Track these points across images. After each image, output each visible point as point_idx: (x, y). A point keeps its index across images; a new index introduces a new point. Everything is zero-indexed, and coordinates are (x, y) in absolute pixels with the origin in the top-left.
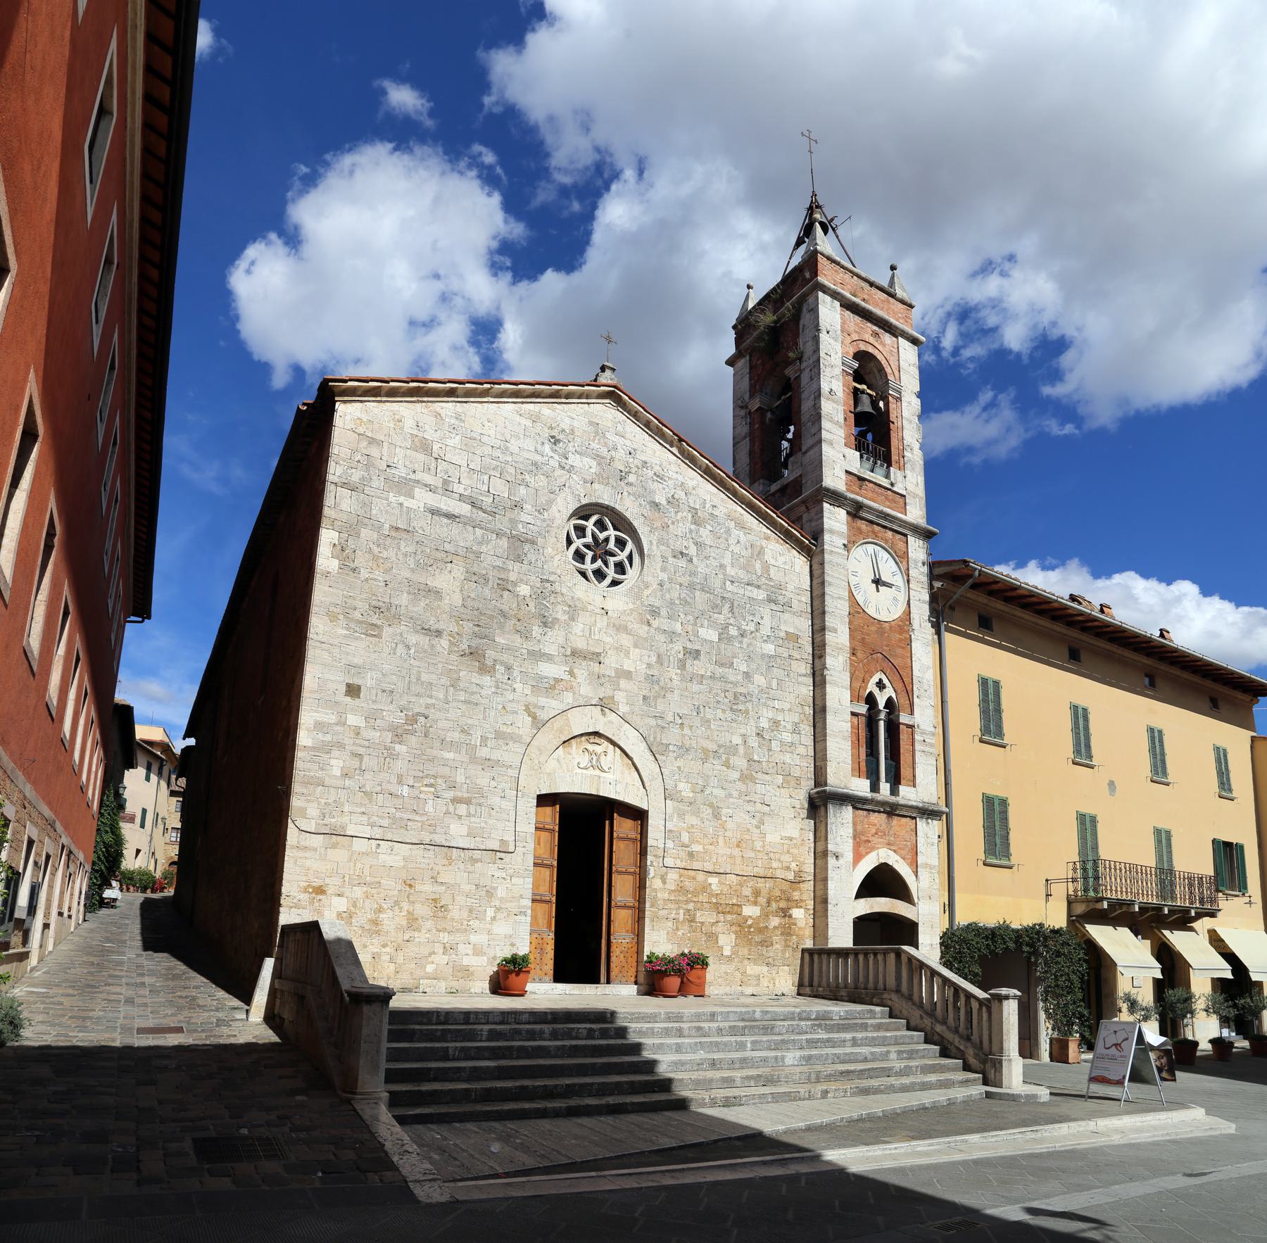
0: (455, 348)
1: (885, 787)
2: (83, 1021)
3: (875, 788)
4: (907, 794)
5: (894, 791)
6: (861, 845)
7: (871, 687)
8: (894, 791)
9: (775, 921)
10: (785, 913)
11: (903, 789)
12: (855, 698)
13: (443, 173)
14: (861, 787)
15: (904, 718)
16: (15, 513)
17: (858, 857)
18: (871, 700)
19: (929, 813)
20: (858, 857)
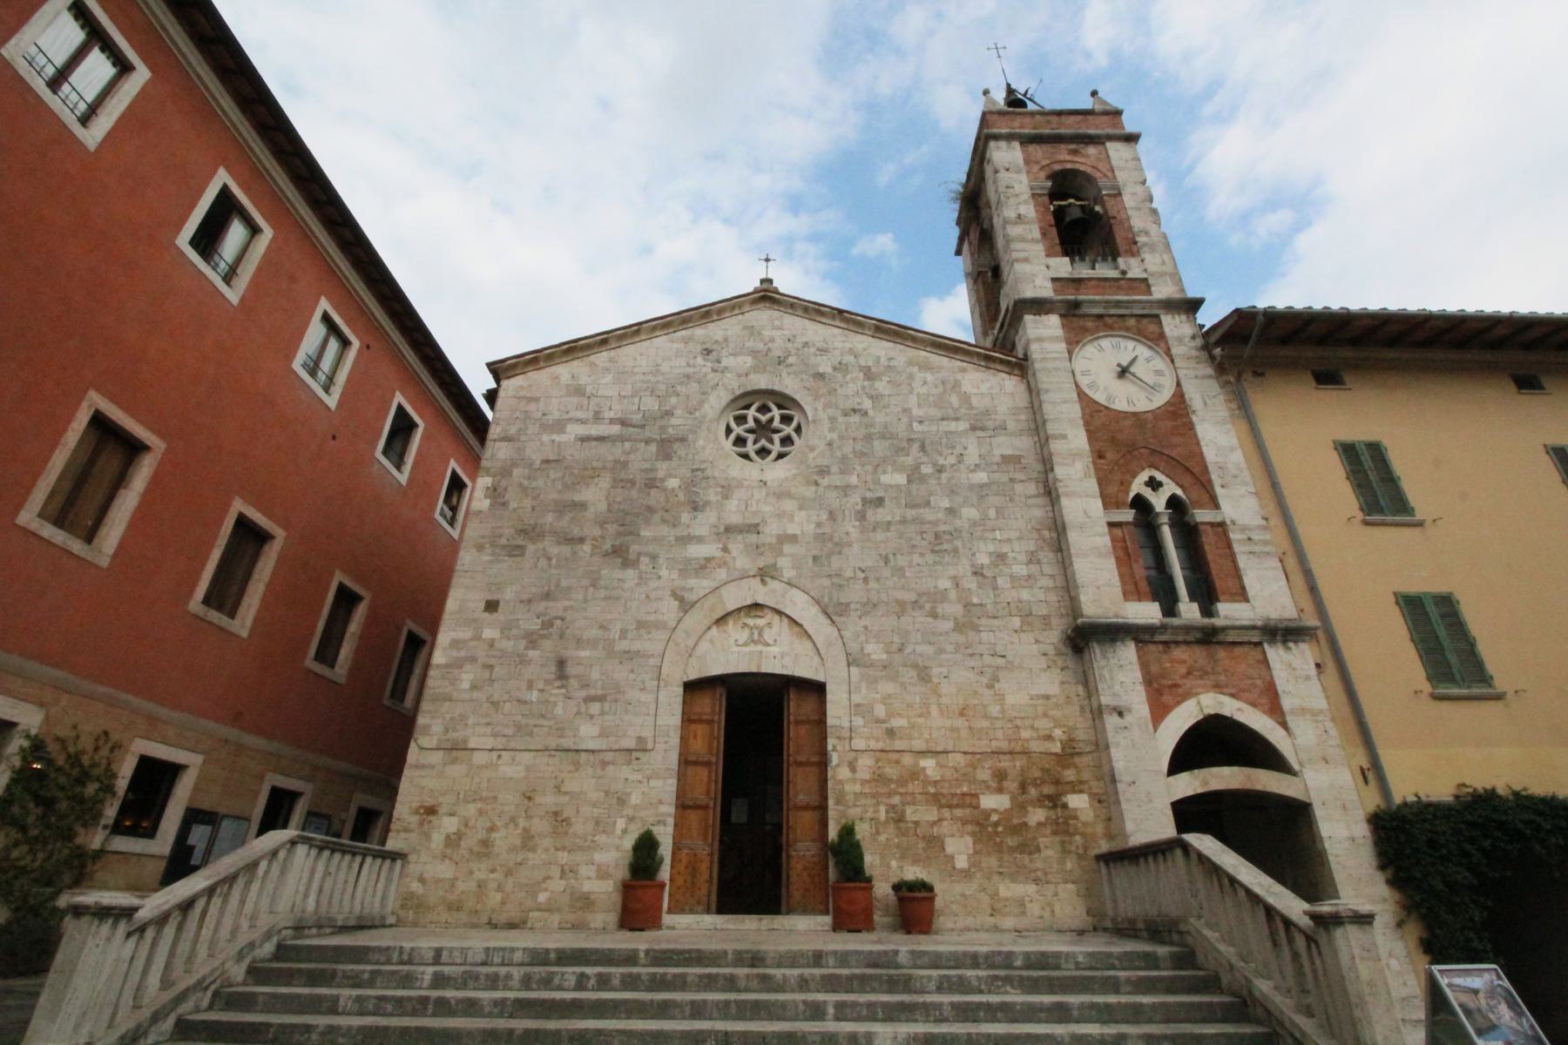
3: (1170, 609)
4: (1229, 612)
5: (1207, 611)
7: (1138, 486)
9: (1037, 815)
10: (1054, 802)
12: (1109, 502)
14: (1147, 612)
18: (1140, 504)
20: (1159, 711)
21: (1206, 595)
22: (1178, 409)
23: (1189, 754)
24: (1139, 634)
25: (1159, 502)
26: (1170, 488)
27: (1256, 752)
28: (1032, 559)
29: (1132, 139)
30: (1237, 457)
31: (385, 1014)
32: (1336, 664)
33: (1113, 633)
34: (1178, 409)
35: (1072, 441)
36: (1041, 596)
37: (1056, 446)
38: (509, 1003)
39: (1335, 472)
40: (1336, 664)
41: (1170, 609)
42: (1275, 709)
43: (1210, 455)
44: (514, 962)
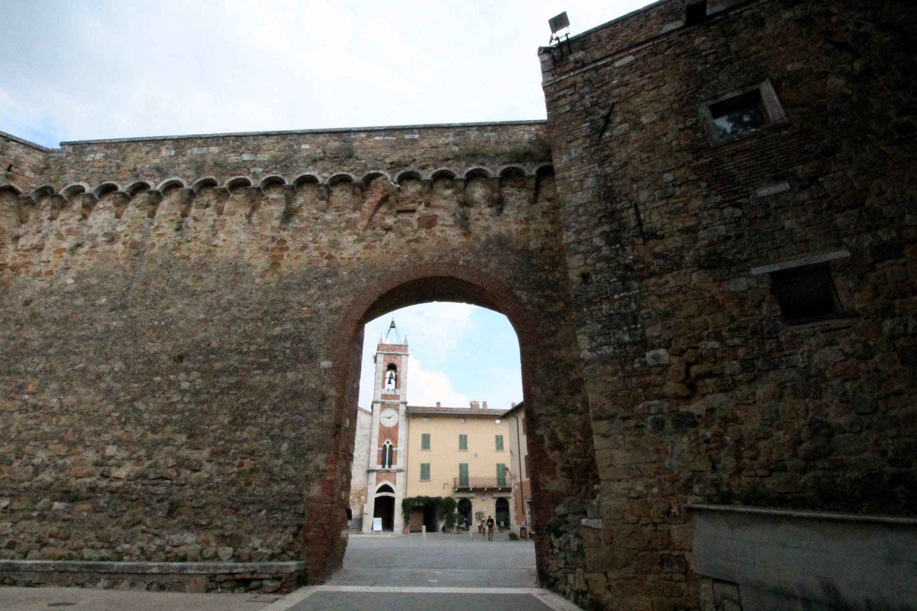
0: (651, 431)
1: (387, 466)
2: (711, 372)
3: (384, 467)
4: (394, 467)
5: (390, 467)
6: (378, 480)
7: (385, 443)
8: (390, 467)
9: (356, 500)
10: (359, 497)
11: (392, 466)
12: (379, 446)
13: (454, 264)
14: (380, 467)
15: (394, 449)
16: (48, 249)
17: (377, 484)
18: (385, 446)
19: (400, 471)
20: (377, 484)
21: (390, 464)
22: (396, 427)
23: (380, 490)
24: (377, 471)
25: (388, 446)
26: (391, 443)
27: (390, 490)
28: (365, 456)
29: (407, 355)
30: (404, 437)
31: (134, 561)
32: (406, 477)
33: (373, 471)
34: (396, 427)
35: (376, 433)
36: (364, 463)
37: (373, 434)
38: (574, 353)
39: (420, 438)
40: (406, 477)
41: (384, 467)
42: (395, 483)
43: (399, 436)
44: (710, 581)
